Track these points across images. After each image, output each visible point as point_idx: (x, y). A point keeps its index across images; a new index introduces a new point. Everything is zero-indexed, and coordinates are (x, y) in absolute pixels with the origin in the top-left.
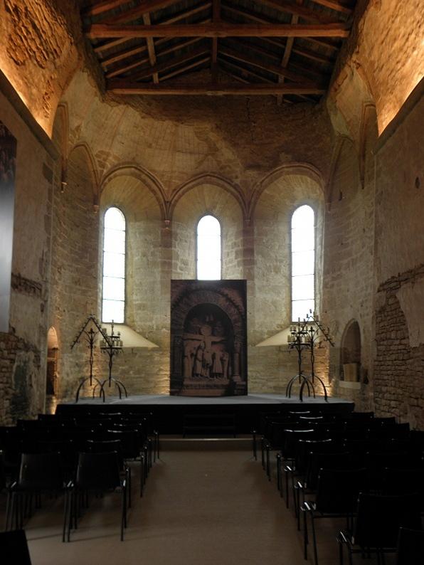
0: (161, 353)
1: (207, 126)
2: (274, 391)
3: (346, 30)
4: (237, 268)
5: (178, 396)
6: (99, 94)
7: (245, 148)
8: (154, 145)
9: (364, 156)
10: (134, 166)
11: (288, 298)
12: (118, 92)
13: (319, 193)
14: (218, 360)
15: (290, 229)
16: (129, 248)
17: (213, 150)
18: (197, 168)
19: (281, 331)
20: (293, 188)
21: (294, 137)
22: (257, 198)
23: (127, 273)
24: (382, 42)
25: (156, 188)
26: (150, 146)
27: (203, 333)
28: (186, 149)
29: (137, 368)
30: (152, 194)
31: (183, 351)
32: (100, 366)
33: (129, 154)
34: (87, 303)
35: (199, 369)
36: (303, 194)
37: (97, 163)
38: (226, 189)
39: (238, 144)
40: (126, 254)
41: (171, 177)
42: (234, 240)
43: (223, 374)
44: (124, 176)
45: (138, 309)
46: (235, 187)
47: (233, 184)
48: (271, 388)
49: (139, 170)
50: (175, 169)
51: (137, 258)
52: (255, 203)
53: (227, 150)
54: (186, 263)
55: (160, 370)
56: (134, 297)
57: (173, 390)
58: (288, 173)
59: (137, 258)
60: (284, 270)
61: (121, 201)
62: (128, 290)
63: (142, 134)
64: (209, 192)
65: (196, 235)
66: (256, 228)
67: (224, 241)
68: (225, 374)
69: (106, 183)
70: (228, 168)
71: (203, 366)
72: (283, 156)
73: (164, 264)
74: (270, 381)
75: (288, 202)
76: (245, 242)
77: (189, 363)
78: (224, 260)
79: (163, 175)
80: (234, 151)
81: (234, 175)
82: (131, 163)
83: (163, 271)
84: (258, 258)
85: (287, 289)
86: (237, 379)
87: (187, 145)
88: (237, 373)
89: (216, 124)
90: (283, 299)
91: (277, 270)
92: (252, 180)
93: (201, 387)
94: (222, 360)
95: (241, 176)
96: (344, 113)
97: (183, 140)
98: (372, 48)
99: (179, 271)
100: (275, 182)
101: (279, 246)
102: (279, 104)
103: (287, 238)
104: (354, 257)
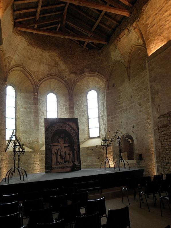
0: (34, 153)
1: (55, 54)
2: (86, 167)
3: (130, 13)
4: (66, 115)
5: (49, 173)
6: (13, 26)
7: (70, 65)
8: (32, 59)
9: (130, 67)
10: (21, 66)
11: (88, 128)
12: (20, 29)
13: (102, 84)
14: (67, 155)
15: (87, 99)
16: (17, 105)
17: (56, 65)
18: (49, 72)
19: (86, 141)
20: (89, 83)
21: (90, 62)
22: (75, 86)
23: (17, 117)
24: (156, 14)
25: (31, 79)
26: (30, 59)
27: (60, 142)
28: (45, 63)
29: (24, 161)
30: (29, 81)
31: (51, 152)
32: (7, 161)
33: (21, 61)
34: (2, 129)
35: (59, 159)
36: (93, 85)
37: (7, 62)
38: (61, 82)
39: (67, 63)
40: (16, 108)
41: (38, 74)
42: (64, 103)
43: (70, 161)
44: (17, 71)
45: (23, 133)
46: (65, 81)
47: (64, 80)
48: (85, 166)
49: (24, 69)
50: (40, 71)
51: (21, 110)
52: (74, 88)
53: (63, 65)
54: (43, 112)
55: (34, 161)
56: (20, 128)
57: (46, 171)
58: (88, 76)
59: (21, 110)
60: (86, 116)
61: (14, 83)
62: (17, 124)
63: (27, 53)
64: (53, 82)
65: (46, 101)
66: (74, 98)
67: (59, 104)
68: (71, 161)
69: (10, 73)
70: (62, 73)
71: (61, 158)
72: (86, 69)
73: (35, 112)
74: (84, 163)
75: (86, 89)
76: (70, 104)
77: (54, 157)
78: (59, 112)
79: (35, 73)
80: (66, 66)
81: (65, 76)
82: (21, 65)
83: (34, 116)
84: (76, 111)
85: (87, 124)
86: (76, 163)
87: (46, 61)
88: (76, 160)
89: (59, 54)
90: (86, 128)
91: (83, 116)
92: (73, 78)
93: (61, 168)
94: (69, 154)
95: (67, 75)
96: (121, 50)
97: (44, 58)
98: (149, 18)
99: (41, 116)
100: (82, 80)
101: (83, 106)
102: (83, 49)
103: (86, 103)
104: (124, 108)
